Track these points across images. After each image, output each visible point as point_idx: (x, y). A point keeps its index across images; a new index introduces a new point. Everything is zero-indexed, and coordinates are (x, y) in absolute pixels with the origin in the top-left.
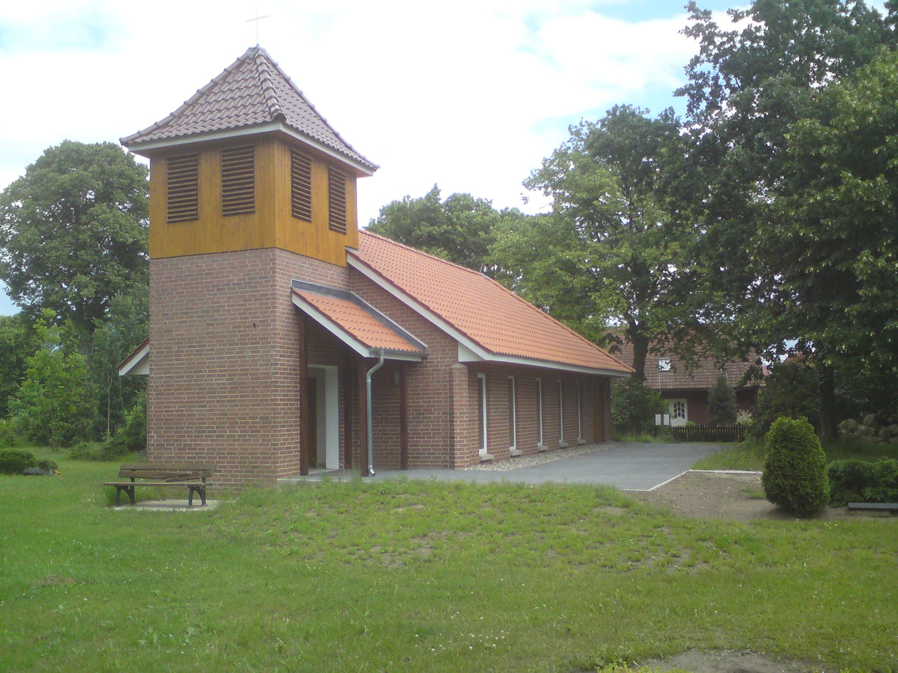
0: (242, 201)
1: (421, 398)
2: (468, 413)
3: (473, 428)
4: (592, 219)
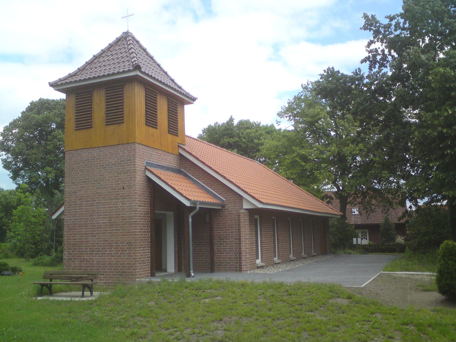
0: (117, 116)
1: (222, 230)
2: (250, 239)
3: (252, 248)
4: (315, 133)
